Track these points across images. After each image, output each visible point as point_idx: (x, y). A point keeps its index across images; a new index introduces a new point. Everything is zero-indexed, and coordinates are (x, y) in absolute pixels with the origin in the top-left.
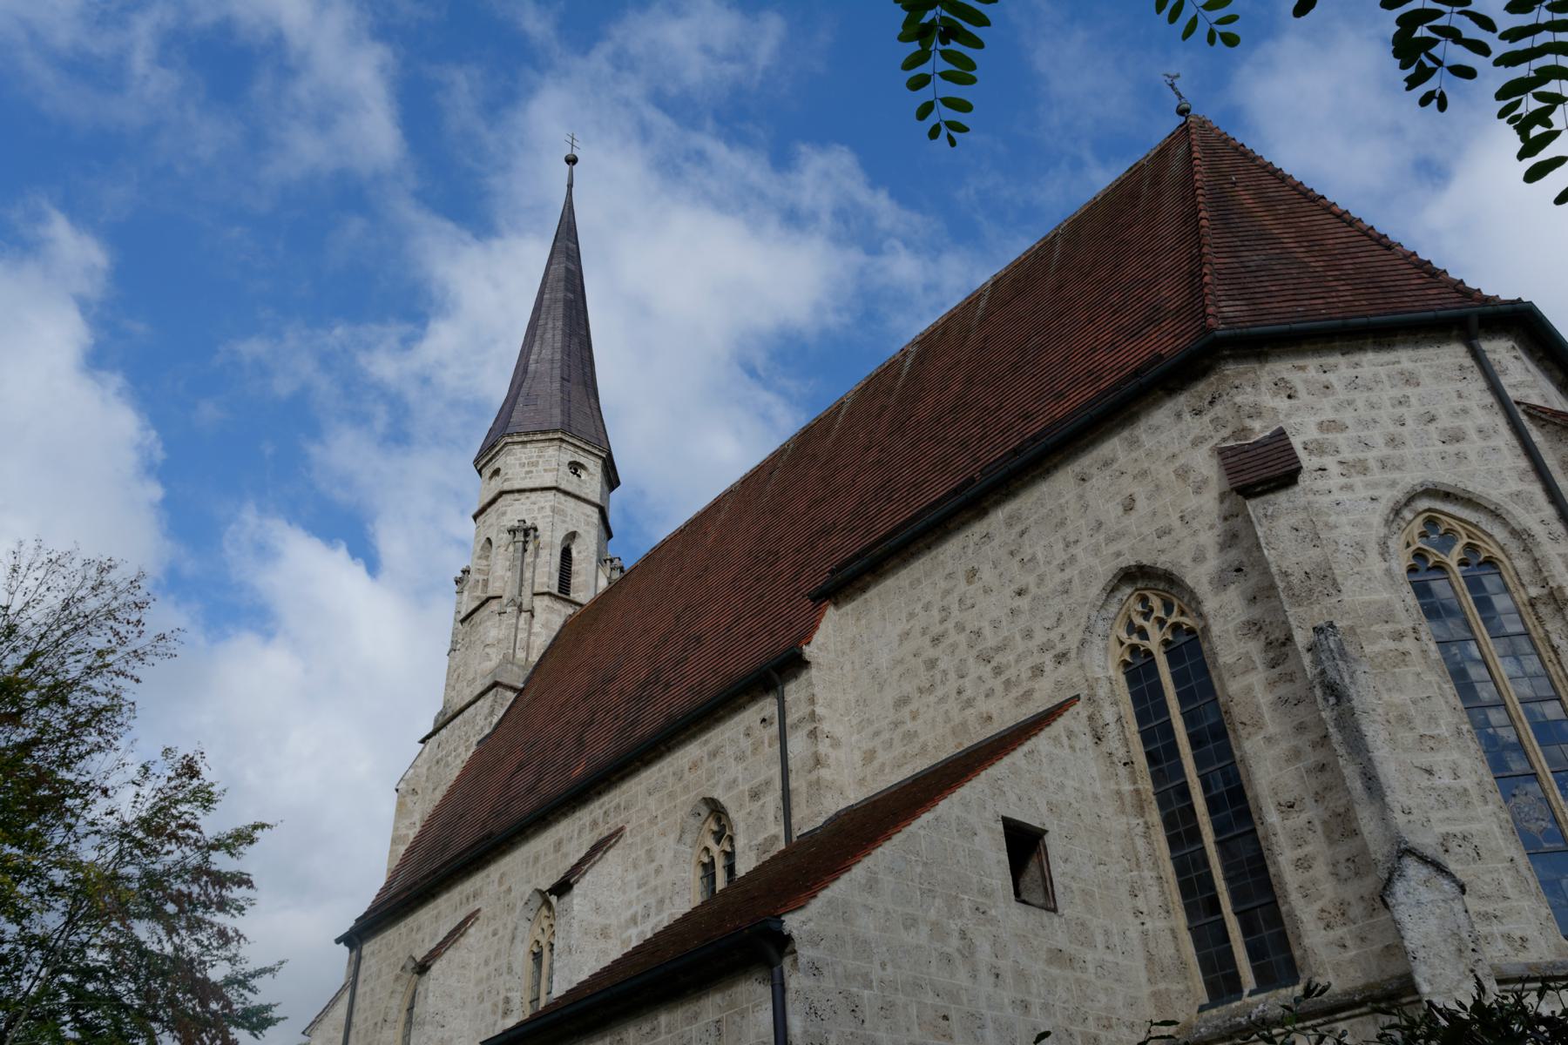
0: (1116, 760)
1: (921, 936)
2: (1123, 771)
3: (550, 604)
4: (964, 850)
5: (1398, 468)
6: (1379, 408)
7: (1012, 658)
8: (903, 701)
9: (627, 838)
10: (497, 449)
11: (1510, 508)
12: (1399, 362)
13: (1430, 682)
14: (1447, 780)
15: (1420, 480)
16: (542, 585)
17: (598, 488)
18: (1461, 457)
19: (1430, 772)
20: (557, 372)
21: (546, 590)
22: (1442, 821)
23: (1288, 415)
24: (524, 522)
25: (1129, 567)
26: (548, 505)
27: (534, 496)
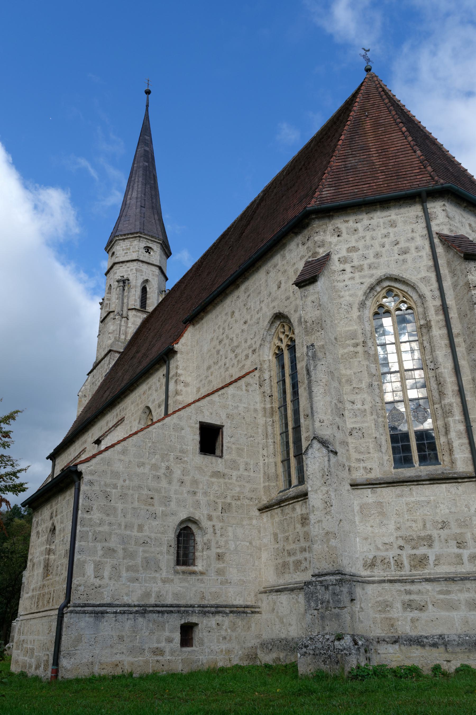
0: (266, 395)
1: (147, 470)
2: (268, 399)
3: (135, 313)
4: (175, 436)
5: (376, 268)
6: (376, 239)
7: (240, 351)
8: (209, 368)
9: (126, 422)
10: (113, 243)
11: (418, 285)
12: (390, 216)
13: (364, 365)
14: (359, 406)
15: (384, 273)
16: (132, 305)
17: (158, 258)
18: (404, 261)
19: (353, 403)
20: (139, 203)
21: (133, 307)
22: (352, 423)
23: (336, 245)
24: (123, 277)
25: (276, 313)
26: (134, 268)
27: (128, 264)
